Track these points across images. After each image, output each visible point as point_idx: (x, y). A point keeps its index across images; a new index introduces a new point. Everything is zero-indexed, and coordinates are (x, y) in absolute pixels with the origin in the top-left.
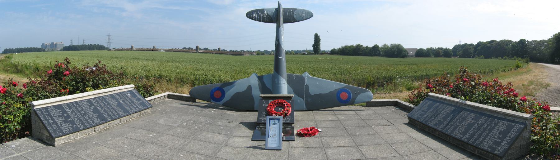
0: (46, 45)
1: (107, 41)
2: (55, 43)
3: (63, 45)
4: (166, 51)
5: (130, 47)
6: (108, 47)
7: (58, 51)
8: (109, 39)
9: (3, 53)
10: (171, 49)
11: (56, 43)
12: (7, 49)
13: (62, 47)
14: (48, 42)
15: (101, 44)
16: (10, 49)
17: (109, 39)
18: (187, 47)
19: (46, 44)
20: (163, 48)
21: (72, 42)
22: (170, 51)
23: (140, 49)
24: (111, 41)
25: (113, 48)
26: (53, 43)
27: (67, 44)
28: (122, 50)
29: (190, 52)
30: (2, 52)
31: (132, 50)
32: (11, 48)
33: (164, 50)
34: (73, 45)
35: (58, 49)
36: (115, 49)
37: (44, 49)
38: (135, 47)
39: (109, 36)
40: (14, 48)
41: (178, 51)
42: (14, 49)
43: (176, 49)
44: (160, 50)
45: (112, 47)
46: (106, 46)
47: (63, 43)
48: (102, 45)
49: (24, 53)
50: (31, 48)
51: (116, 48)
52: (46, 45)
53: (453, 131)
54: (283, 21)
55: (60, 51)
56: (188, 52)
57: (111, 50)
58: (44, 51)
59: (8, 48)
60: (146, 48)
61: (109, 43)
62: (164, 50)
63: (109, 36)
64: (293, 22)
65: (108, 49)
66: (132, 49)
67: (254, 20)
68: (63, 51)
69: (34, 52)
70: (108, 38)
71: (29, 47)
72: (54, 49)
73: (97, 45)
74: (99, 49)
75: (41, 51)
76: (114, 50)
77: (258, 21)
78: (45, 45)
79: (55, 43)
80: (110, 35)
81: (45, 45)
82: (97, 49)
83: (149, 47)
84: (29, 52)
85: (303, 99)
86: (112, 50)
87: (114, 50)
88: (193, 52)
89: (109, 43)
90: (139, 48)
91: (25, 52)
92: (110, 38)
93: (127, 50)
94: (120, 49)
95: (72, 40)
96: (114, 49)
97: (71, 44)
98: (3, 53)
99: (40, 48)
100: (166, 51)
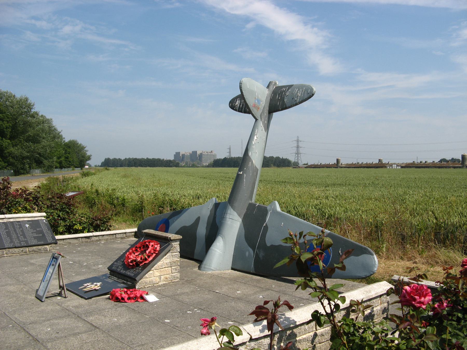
0: (183, 155)
1: (295, 150)
2: (198, 153)
3: (215, 155)
4: (402, 167)
5: (334, 161)
6: (296, 161)
7: (203, 167)
8: (298, 147)
9: (101, 166)
10: (411, 164)
11: (201, 152)
12: (109, 159)
13: (211, 161)
14: (186, 150)
15: (283, 155)
16: (115, 159)
17: (298, 147)
18: (448, 158)
19: (184, 153)
20: (397, 162)
21: (230, 152)
22: (411, 167)
23: (352, 164)
24: (301, 150)
25: (303, 163)
26: (195, 153)
27: (221, 155)
28: (319, 168)
29: (450, 167)
30: (100, 165)
31: (337, 168)
32: (117, 158)
33: (397, 166)
34: (232, 157)
35: (205, 164)
36: (307, 164)
37: (178, 164)
38: (344, 162)
39: (298, 141)
40: (123, 158)
41: (424, 167)
42: (123, 159)
43: (421, 162)
44: (391, 165)
45: (303, 161)
46: (292, 159)
47: (214, 153)
48: (284, 157)
49: (139, 168)
50: (153, 159)
51: (309, 164)
52: (182, 155)
53: (108, 274)
54: (268, 109)
55: (208, 166)
56: (446, 167)
57: (299, 167)
58: (177, 165)
59: (111, 158)
60: (365, 162)
61: (298, 153)
62: (397, 166)
63: (298, 141)
64: (282, 110)
65: (296, 165)
66: (337, 165)
67: (235, 110)
68: (213, 167)
69: (159, 166)
70: (296, 145)
71: (151, 157)
72: (195, 163)
73: (275, 157)
74: (279, 166)
75: (171, 167)
76: (305, 167)
77: (239, 111)
78: (181, 155)
79: (198, 153)
80: (300, 139)
81: (181, 155)
82: (274, 165)
83: (370, 161)
84: (150, 166)
85: (254, 251)
86: (302, 167)
87: (305, 167)
88: (454, 167)
89: (298, 153)
90: (350, 162)
91: (142, 166)
92: (300, 144)
93: (328, 166)
94: (316, 165)
95: (230, 149)
96: (304, 164)
97: (228, 154)
98: (101, 166)
99: (170, 161)
100: (402, 167)
